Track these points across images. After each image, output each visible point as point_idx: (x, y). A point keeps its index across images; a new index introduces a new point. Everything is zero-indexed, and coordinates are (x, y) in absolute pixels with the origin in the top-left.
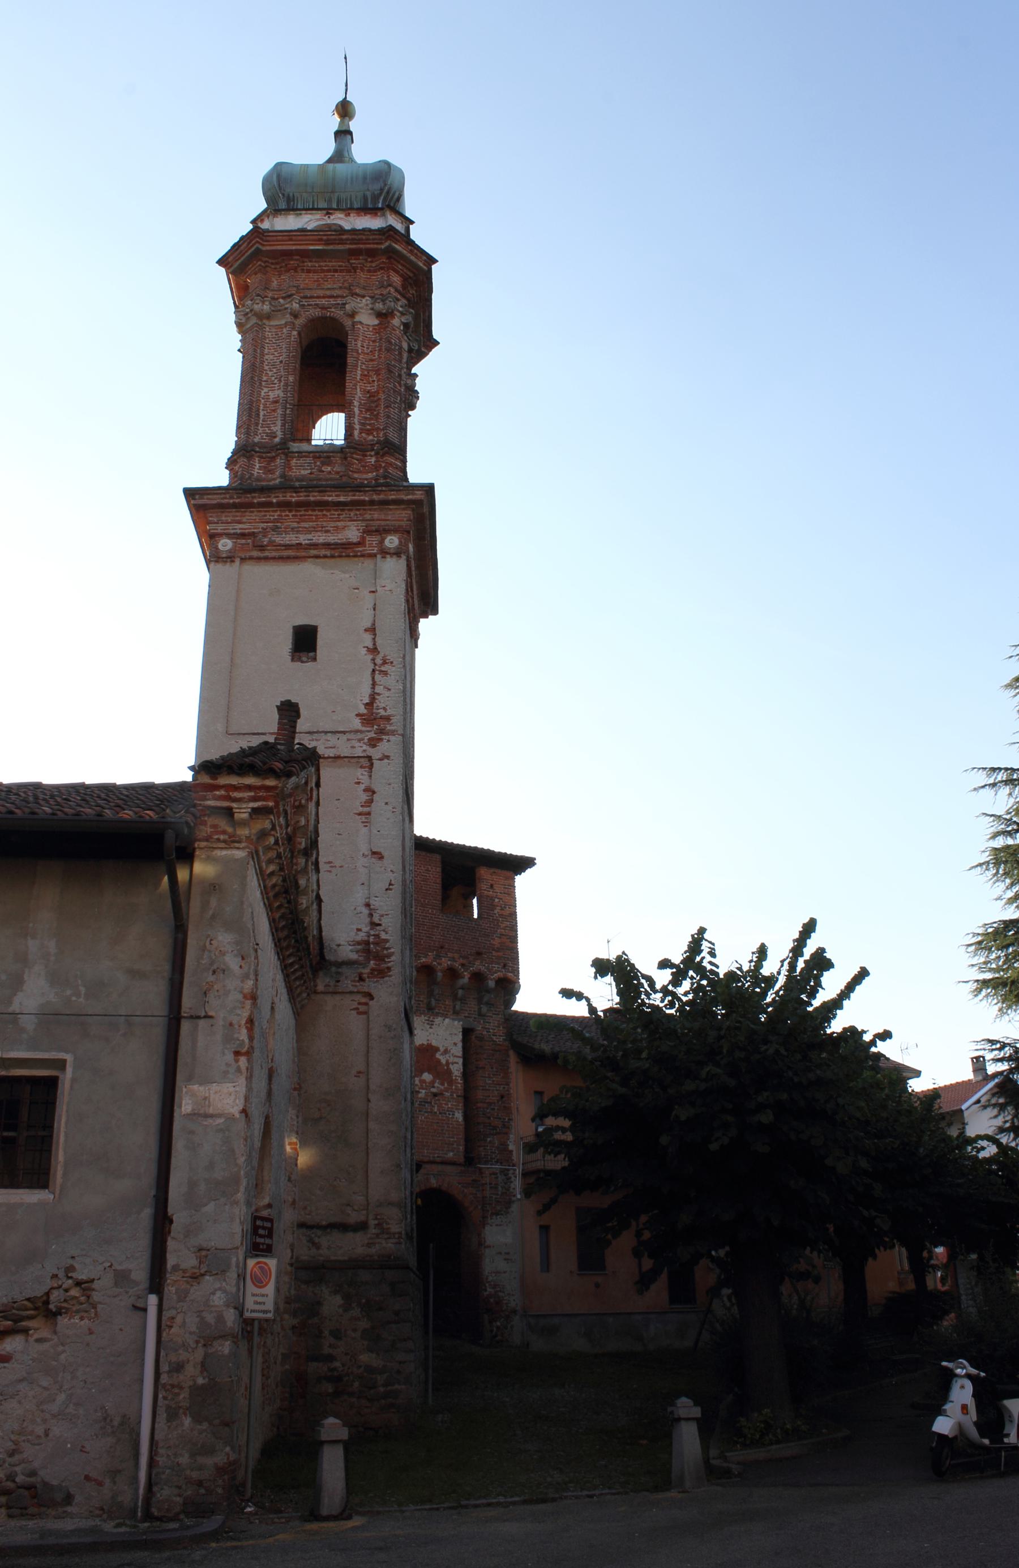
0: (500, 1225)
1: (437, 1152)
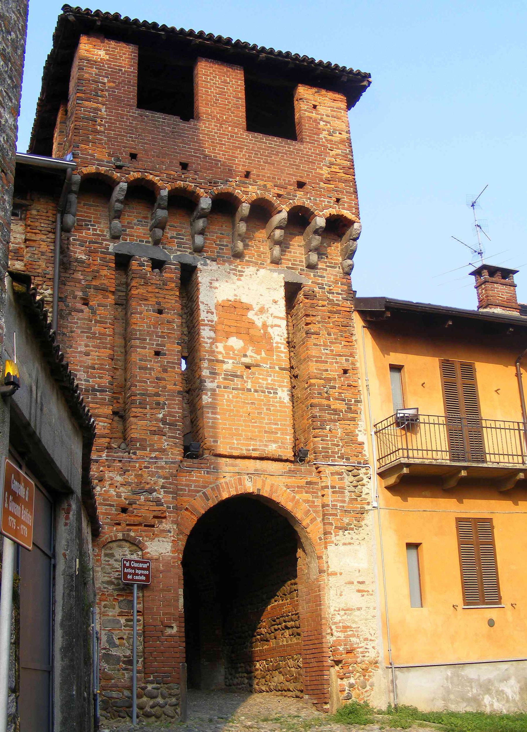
0: (350, 544)
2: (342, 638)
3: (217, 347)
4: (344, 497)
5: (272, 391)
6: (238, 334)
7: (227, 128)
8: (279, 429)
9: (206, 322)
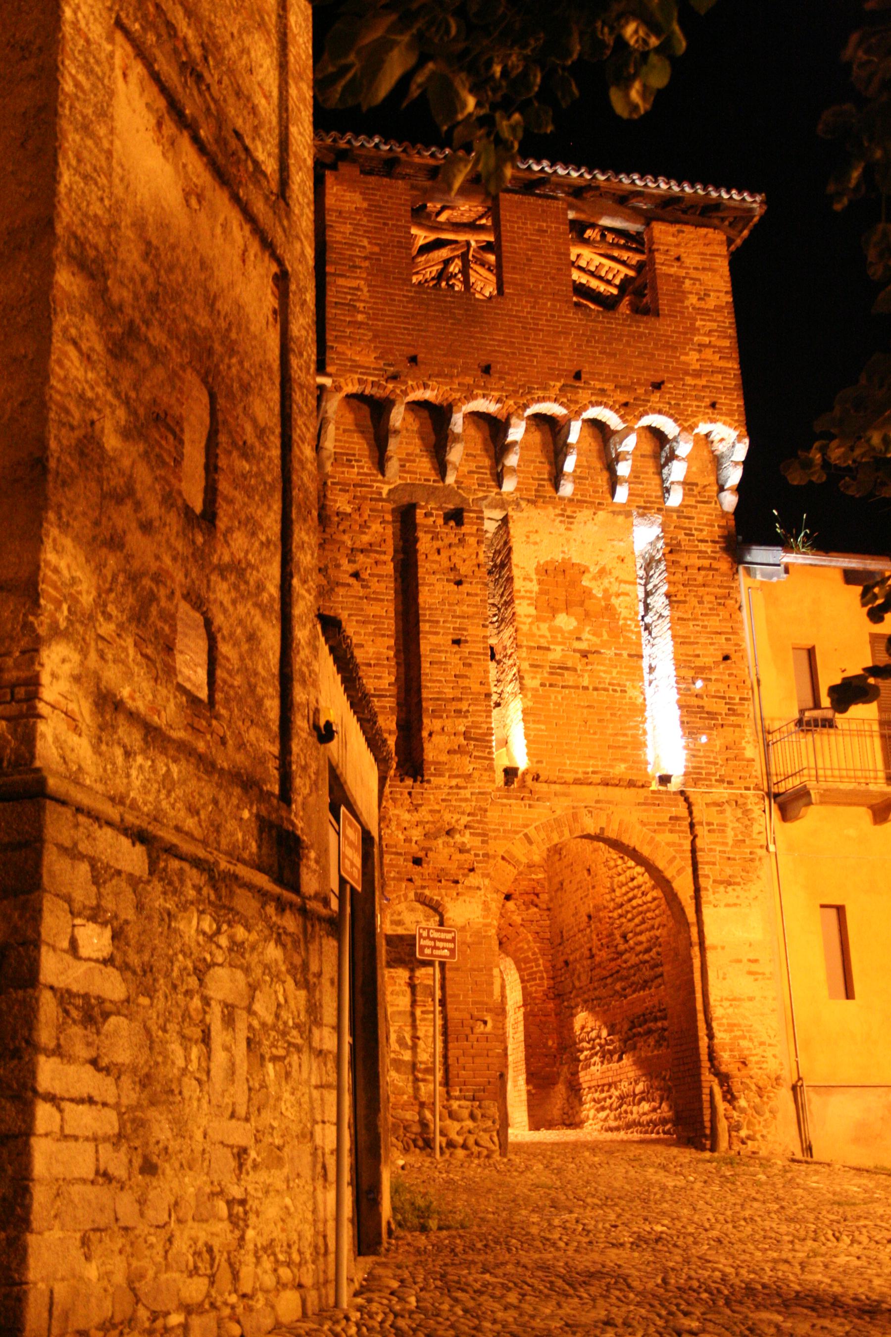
0: (735, 905)
1: (591, 762)
2: (727, 1041)
3: (539, 629)
4: (726, 837)
5: (618, 689)
6: (568, 607)
7: (546, 304)
8: (629, 743)
9: (523, 593)
